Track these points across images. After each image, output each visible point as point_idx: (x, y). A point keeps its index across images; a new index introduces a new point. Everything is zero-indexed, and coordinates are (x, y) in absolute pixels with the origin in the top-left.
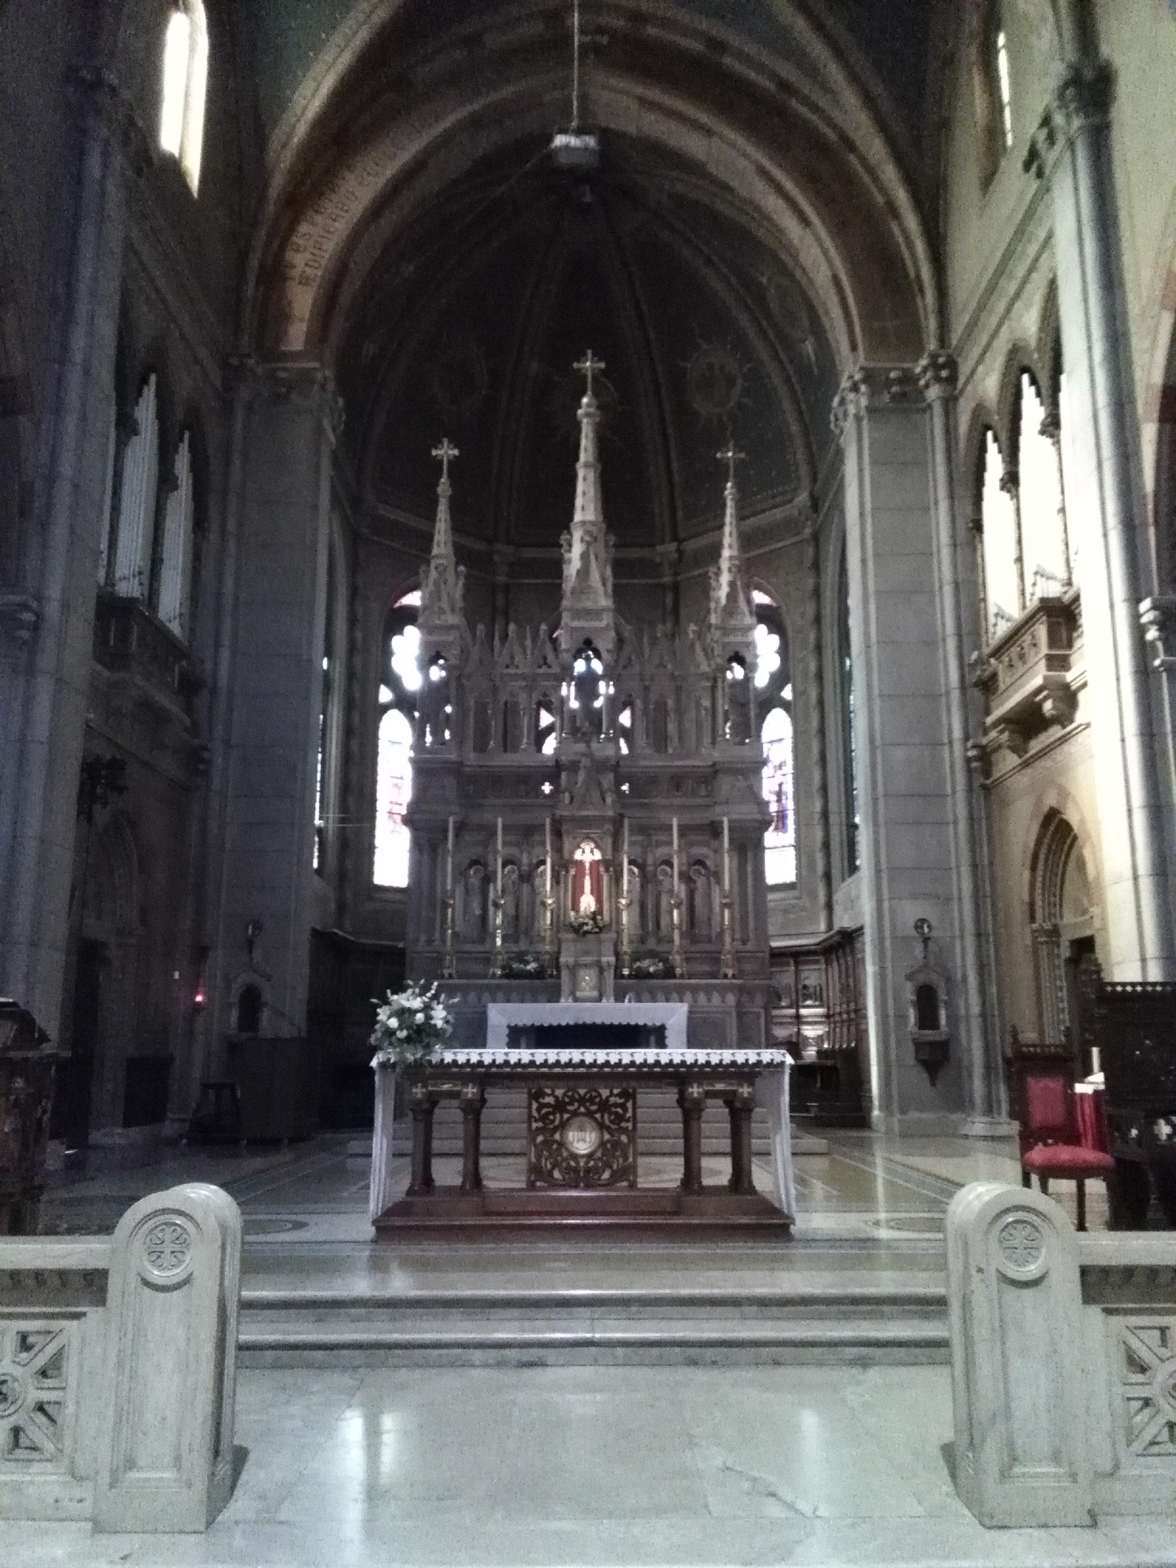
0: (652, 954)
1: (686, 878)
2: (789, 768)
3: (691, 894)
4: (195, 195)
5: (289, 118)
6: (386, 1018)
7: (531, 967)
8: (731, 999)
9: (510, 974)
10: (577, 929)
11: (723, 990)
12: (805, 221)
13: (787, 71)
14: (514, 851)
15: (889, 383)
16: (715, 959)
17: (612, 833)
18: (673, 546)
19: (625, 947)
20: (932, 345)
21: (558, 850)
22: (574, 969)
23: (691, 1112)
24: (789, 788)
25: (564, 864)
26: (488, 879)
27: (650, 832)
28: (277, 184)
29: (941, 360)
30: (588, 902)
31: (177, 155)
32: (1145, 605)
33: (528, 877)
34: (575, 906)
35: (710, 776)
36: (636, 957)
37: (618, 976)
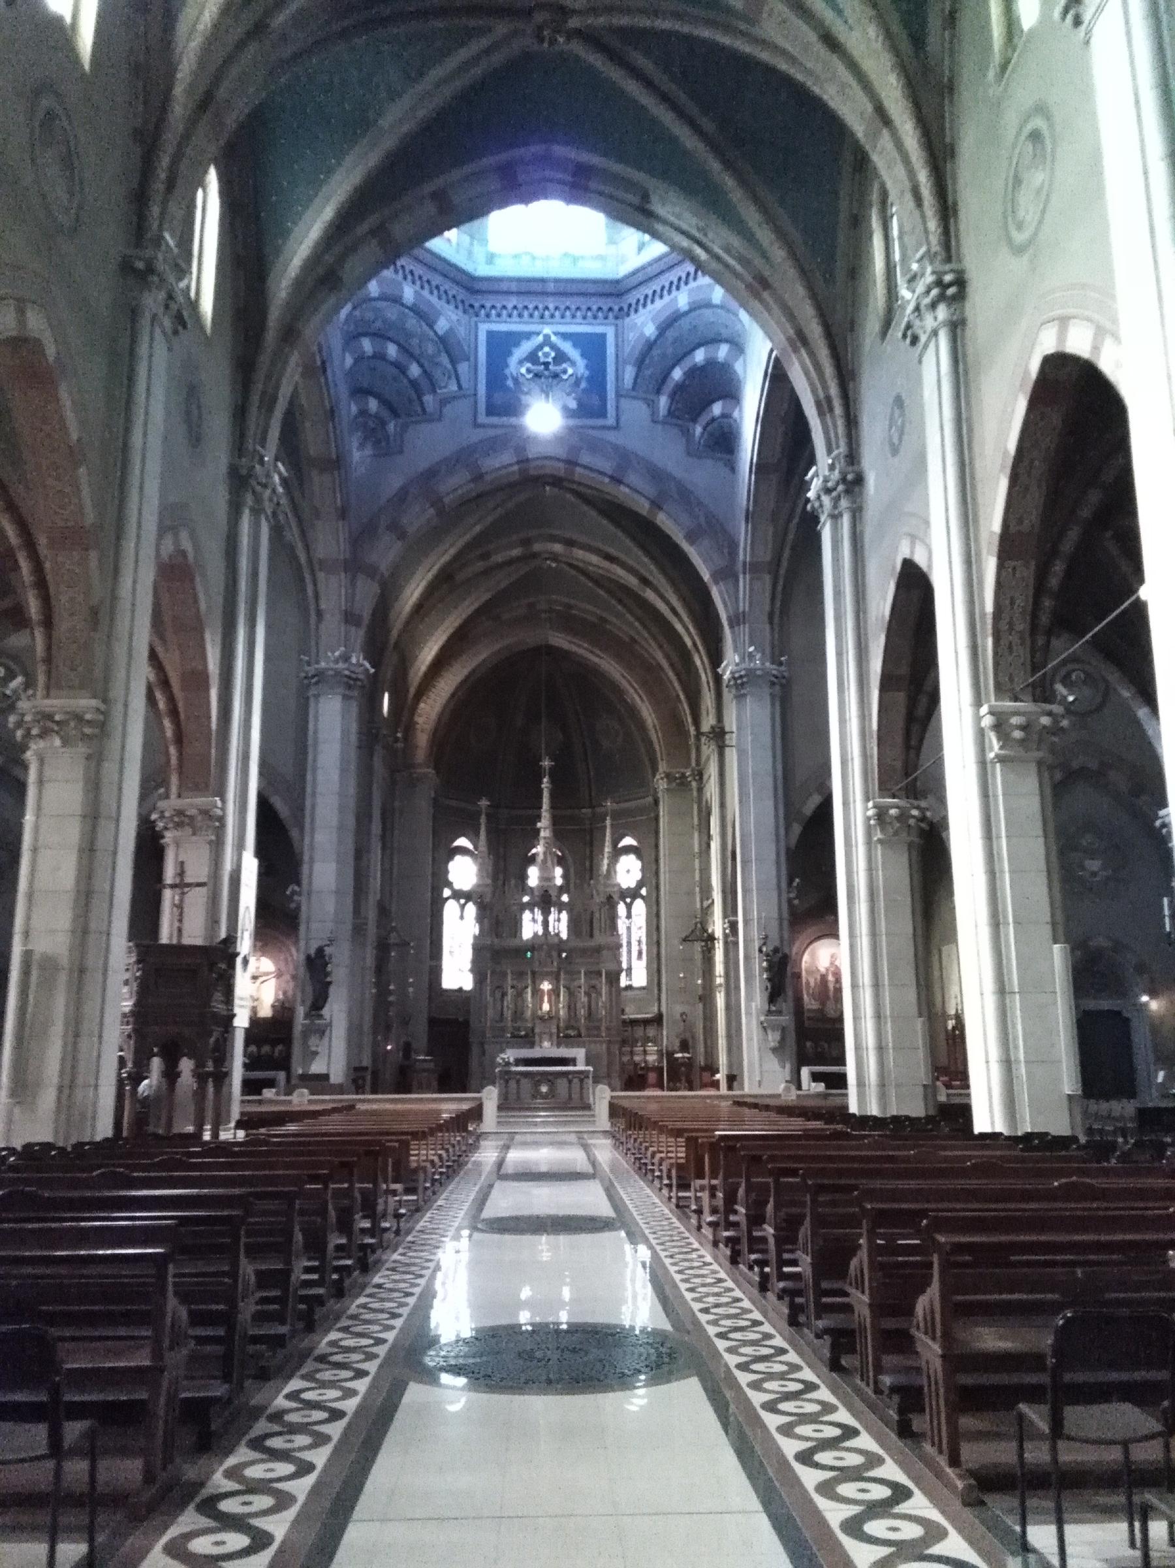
0: (573, 1028)
1: (588, 994)
2: (644, 930)
3: (589, 1002)
4: (87, 67)
5: (417, 663)
6: (499, 1060)
7: (523, 1033)
8: (604, 1046)
9: (513, 1036)
10: (541, 1018)
11: (601, 1042)
12: (642, 700)
13: (632, 633)
14: (515, 982)
15: (676, 778)
16: (598, 1028)
17: (555, 978)
18: (589, 810)
19: (562, 1025)
20: (693, 764)
21: (534, 982)
22: (541, 1035)
23: (570, 1082)
24: (644, 940)
25: (537, 993)
26: (504, 995)
27: (573, 975)
28: (412, 690)
29: (948, 278)
30: (546, 1007)
31: (68, 19)
32: (984, 709)
33: (520, 994)
34: (541, 1009)
35: (598, 950)
36: (567, 1028)
37: (558, 1037)
